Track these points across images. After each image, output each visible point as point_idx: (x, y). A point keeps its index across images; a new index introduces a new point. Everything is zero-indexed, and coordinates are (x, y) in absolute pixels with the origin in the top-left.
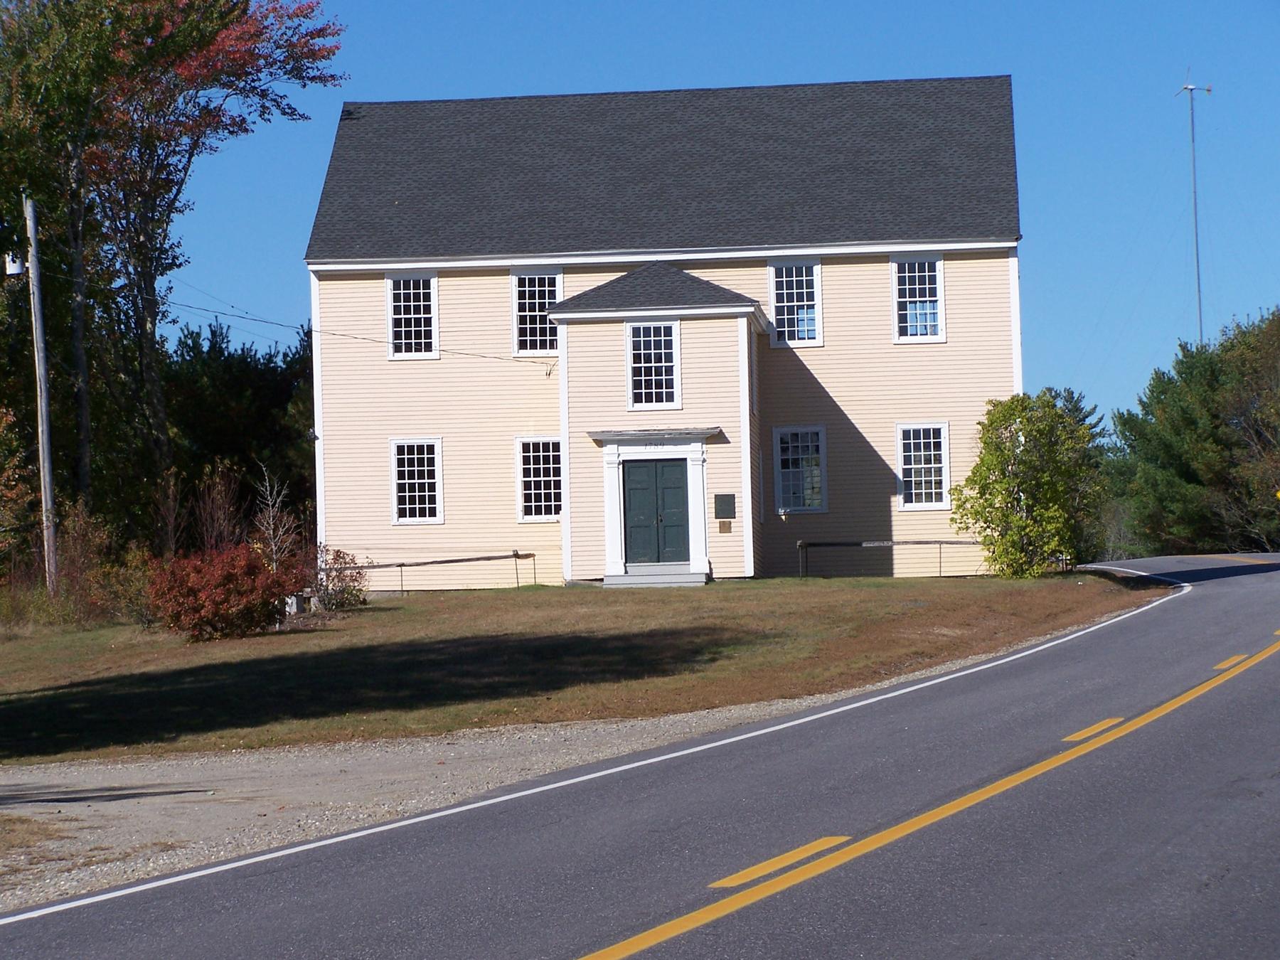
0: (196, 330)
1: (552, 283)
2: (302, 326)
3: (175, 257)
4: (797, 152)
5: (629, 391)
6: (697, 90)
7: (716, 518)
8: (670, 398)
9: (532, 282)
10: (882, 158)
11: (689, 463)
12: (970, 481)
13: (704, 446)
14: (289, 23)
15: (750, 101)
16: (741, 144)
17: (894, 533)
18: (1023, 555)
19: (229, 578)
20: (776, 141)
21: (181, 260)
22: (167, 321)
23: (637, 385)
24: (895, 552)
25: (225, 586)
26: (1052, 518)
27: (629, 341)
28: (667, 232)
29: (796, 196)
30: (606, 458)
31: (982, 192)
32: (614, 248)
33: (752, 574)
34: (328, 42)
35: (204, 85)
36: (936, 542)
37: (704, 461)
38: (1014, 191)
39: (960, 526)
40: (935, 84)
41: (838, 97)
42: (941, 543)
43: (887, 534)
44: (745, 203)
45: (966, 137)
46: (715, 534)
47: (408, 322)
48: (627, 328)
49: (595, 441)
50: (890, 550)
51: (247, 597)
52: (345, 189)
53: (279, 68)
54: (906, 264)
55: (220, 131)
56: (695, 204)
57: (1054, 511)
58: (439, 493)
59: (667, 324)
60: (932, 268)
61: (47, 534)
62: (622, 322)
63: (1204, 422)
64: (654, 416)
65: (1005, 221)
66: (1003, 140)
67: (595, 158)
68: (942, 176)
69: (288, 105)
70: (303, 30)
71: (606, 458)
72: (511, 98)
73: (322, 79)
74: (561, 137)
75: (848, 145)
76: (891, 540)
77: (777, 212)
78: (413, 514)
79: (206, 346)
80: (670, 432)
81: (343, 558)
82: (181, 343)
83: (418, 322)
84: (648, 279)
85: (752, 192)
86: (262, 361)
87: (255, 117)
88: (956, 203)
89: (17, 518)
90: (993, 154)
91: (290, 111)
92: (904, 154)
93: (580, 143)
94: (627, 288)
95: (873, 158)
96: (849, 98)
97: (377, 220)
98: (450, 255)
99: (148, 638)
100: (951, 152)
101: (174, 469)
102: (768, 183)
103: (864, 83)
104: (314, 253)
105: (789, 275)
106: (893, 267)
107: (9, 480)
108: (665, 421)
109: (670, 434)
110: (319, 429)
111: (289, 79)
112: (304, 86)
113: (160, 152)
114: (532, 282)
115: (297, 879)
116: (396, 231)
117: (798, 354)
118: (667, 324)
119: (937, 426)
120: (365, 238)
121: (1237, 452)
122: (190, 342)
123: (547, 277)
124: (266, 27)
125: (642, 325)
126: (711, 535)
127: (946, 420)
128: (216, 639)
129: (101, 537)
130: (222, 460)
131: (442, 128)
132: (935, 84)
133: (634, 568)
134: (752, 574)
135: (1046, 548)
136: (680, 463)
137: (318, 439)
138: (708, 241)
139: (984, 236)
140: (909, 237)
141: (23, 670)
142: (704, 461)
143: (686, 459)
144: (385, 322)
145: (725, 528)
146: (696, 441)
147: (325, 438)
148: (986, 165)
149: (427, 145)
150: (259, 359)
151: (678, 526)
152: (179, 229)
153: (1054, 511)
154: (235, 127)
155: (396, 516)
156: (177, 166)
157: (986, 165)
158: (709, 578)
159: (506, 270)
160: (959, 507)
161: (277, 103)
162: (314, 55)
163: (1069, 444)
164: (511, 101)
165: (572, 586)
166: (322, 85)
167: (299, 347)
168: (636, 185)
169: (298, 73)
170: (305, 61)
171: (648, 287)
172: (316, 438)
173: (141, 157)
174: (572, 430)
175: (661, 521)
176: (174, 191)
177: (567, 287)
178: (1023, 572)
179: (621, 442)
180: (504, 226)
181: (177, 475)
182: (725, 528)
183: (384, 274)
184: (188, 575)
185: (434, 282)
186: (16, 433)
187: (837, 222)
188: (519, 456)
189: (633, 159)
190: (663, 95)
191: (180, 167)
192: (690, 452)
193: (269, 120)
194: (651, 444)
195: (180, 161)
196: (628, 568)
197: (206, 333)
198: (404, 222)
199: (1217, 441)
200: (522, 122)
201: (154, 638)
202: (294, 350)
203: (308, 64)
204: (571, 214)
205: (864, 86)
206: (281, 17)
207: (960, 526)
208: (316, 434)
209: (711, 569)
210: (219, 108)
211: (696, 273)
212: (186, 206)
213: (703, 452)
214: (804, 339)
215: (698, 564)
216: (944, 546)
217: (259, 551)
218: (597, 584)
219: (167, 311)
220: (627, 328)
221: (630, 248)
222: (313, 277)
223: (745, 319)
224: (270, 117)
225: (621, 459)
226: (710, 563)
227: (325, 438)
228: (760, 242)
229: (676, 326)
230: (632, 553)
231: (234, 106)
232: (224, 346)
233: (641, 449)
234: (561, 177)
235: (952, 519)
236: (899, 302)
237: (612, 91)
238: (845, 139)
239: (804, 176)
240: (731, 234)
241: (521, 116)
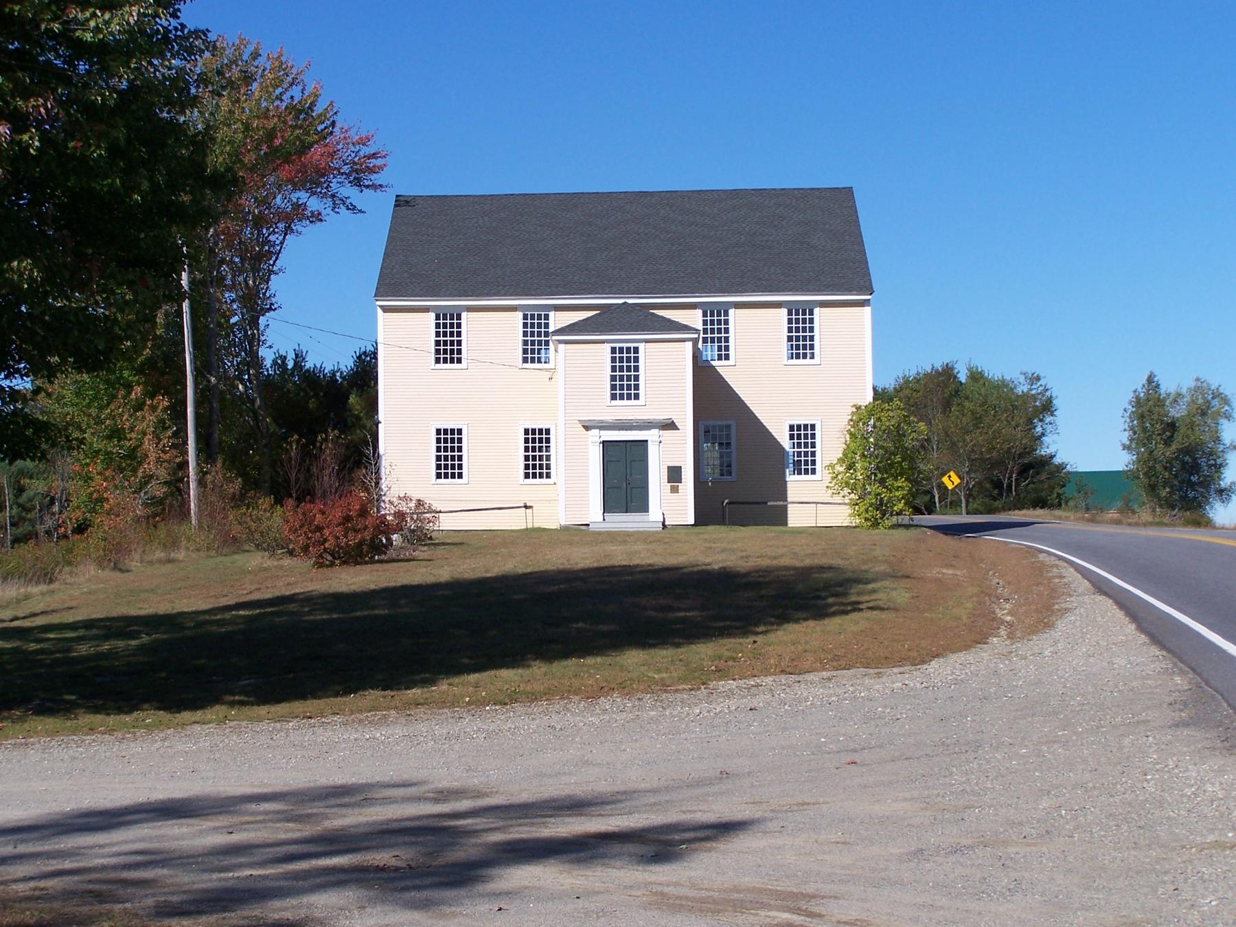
0: (284, 354)
1: (547, 317)
5: (608, 392)
9: (533, 317)
10: (771, 238)
12: (841, 461)
14: (353, 149)
19: (348, 519)
20: (697, 226)
21: (276, 306)
23: (613, 387)
24: (789, 509)
25: (344, 525)
26: (900, 487)
27: (609, 356)
30: (591, 439)
32: (582, 294)
33: (693, 523)
34: (379, 162)
36: (813, 503)
37: (660, 442)
42: (818, 503)
43: (785, 499)
47: (445, 343)
48: (608, 347)
49: (583, 426)
50: (786, 507)
54: (792, 309)
55: (304, 221)
57: (901, 482)
59: (636, 345)
61: (192, 485)
62: (604, 343)
64: (625, 410)
66: (853, 228)
70: (362, 154)
71: (591, 439)
76: (786, 501)
79: (290, 365)
81: (423, 505)
82: (275, 362)
83: (452, 343)
87: (329, 210)
88: (826, 269)
89: (169, 474)
90: (847, 238)
93: (561, 225)
101: (296, 437)
104: (380, 292)
107: (164, 446)
112: (361, 191)
113: (265, 231)
114: (533, 317)
118: (636, 345)
122: (279, 362)
124: (338, 150)
125: (618, 345)
127: (820, 418)
130: (333, 431)
132: (801, 191)
133: (609, 516)
135: (895, 508)
136: (642, 443)
139: (849, 291)
141: (185, 588)
142: (660, 442)
143: (647, 441)
145: (675, 490)
152: (277, 285)
160: (833, 478)
162: (372, 170)
165: (565, 529)
166: (373, 191)
169: (358, 183)
172: (379, 422)
174: (567, 418)
176: (274, 258)
177: (558, 320)
180: (512, 278)
182: (675, 490)
184: (315, 516)
185: (464, 315)
186: (168, 415)
189: (599, 236)
191: (278, 242)
192: (651, 435)
194: (623, 429)
201: (281, 562)
204: (558, 271)
205: (753, 192)
206: (348, 144)
208: (380, 419)
209: (664, 519)
215: (655, 514)
216: (818, 505)
220: (608, 347)
222: (380, 311)
225: (602, 439)
228: (692, 291)
229: (641, 346)
230: (608, 507)
231: (314, 204)
233: (617, 432)
235: (827, 487)
236: (611, 376)
238: (744, 225)
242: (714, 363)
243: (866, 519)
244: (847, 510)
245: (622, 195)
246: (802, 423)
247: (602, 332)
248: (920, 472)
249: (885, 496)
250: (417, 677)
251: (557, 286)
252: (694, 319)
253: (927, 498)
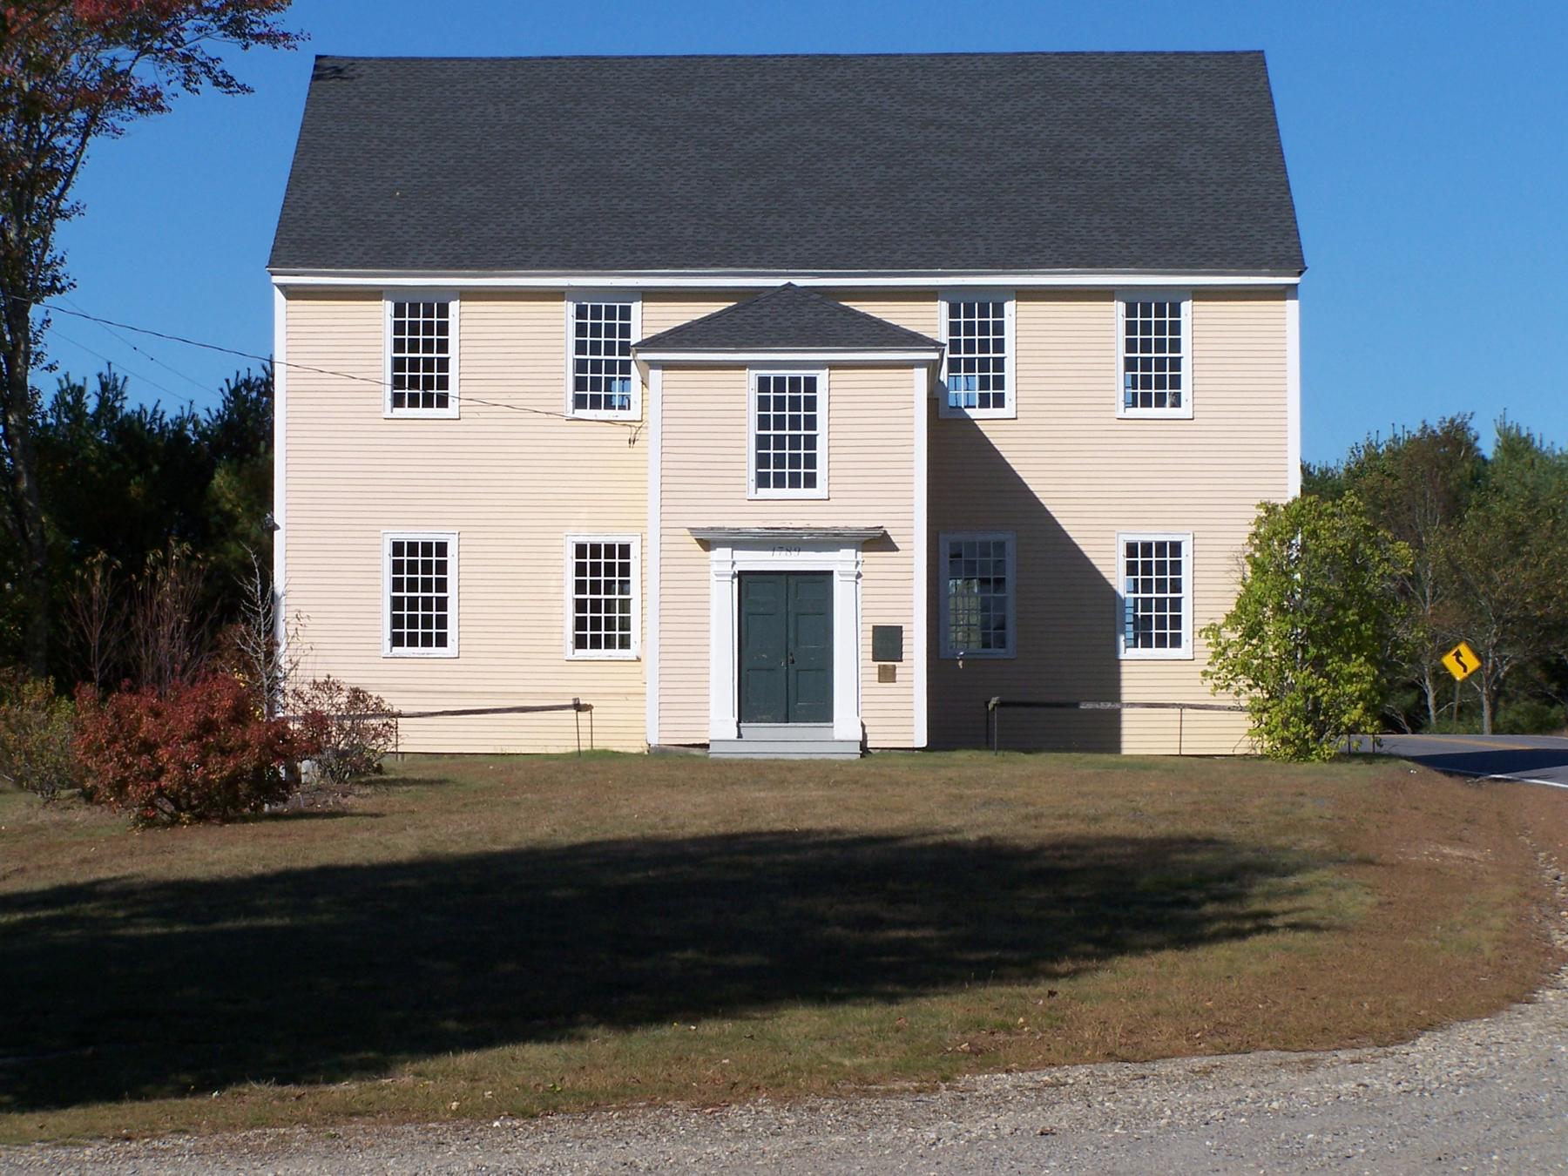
0: (80, 383)
1: (626, 313)
2: (227, 381)
3: (55, 278)
4: (971, 144)
6: (820, 55)
7: (874, 660)
8: (811, 481)
9: (596, 313)
10: (1093, 155)
11: (836, 578)
12: (1233, 619)
13: (859, 553)
15: (896, 73)
16: (888, 129)
17: (1124, 690)
18: (1309, 727)
19: (208, 727)
20: (939, 128)
21: (64, 281)
22: (41, 366)
23: (762, 461)
24: (1124, 718)
25: (200, 738)
26: (1355, 675)
28: (793, 247)
29: (975, 203)
30: (715, 568)
31: (1243, 207)
35: (109, 39)
36: (1174, 706)
37: (859, 576)
38: (1286, 206)
39: (1216, 682)
40: (1159, 59)
41: (1020, 72)
42: (1182, 706)
44: (902, 210)
45: (1211, 132)
46: (872, 684)
48: (751, 377)
50: (1117, 715)
51: (235, 758)
52: (323, 172)
53: (212, 20)
54: (1136, 302)
55: (125, 108)
56: (829, 209)
57: (1357, 665)
58: (451, 613)
60: (1176, 311)
65: (1281, 248)
67: (680, 142)
68: (1182, 183)
69: (222, 72)
71: (715, 568)
72: (555, 58)
73: (272, 38)
74: (631, 112)
75: (1043, 136)
77: (950, 224)
78: (413, 641)
79: (91, 405)
80: (811, 531)
82: (59, 400)
84: (780, 309)
85: (911, 196)
86: (170, 426)
87: (177, 86)
91: (225, 81)
92: (1124, 151)
94: (750, 320)
95: (1082, 155)
96: (1038, 74)
97: (371, 217)
98: (479, 268)
99: (56, 817)
100: (1191, 151)
101: (102, 555)
102: (934, 184)
103: (1057, 54)
106: (1120, 307)
108: (802, 516)
109: (811, 535)
110: (279, 515)
111: (225, 36)
112: (246, 47)
113: (43, 126)
114: (596, 313)
116: (399, 233)
117: (982, 428)
119: (1176, 539)
120: (354, 241)
122: (69, 398)
123: (618, 305)
125: (772, 373)
126: (866, 684)
127: (1189, 530)
128: (184, 823)
129: (1500, 444)
130: (178, 543)
131: (459, 94)
132: (1159, 59)
133: (753, 730)
134: (925, 745)
137: (278, 528)
138: (855, 261)
140: (1146, 265)
142: (859, 576)
144: (382, 362)
145: (887, 676)
146: (847, 545)
147: (289, 527)
148: (1244, 170)
149: (437, 116)
150: (167, 424)
151: (818, 670)
154: (146, 103)
155: (388, 643)
156: (64, 149)
157: (1244, 170)
158: (864, 749)
159: (558, 293)
160: (1216, 655)
161: (209, 68)
164: (555, 61)
165: (659, 754)
167: (222, 409)
168: (743, 180)
169: (237, 29)
170: (249, 12)
171: (780, 320)
173: (16, 132)
175: (793, 662)
176: (60, 184)
178: (1310, 751)
180: (556, 230)
181: (106, 565)
182: (887, 676)
183: (381, 292)
184: (139, 720)
185: (454, 306)
187: (1038, 240)
188: (570, 562)
189: (736, 145)
190: (771, 61)
192: (839, 562)
193: (197, 91)
194: (781, 549)
195: (69, 143)
196: (742, 731)
197: (93, 387)
198: (412, 221)
200: (574, 90)
202: (214, 414)
203: (251, 17)
204: (652, 217)
207: (1216, 682)
209: (864, 735)
210: (126, 72)
212: (75, 209)
213: (858, 563)
214: (974, 407)
215: (845, 725)
217: (242, 685)
218: (696, 751)
219: (42, 352)
220: (751, 377)
221: (742, 266)
222: (279, 296)
223: (925, 370)
224: (198, 86)
225: (737, 569)
226: (863, 726)
227: (289, 527)
229: (822, 377)
231: (146, 72)
232: (118, 404)
234: (634, 166)
235: (1205, 673)
237: (698, 53)
239: (984, 176)
240: (886, 253)
241: (570, 82)
243: (1284, 741)
244: (1245, 722)
248: (1397, 646)
249: (1324, 693)
252: (933, 320)
253: (1410, 698)
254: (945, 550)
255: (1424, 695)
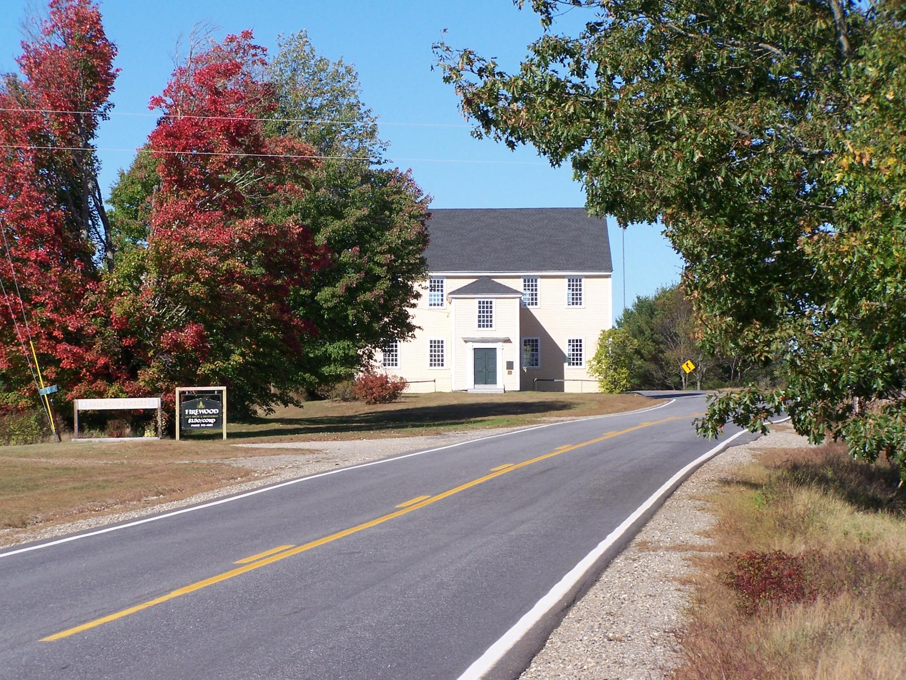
27: (478, 305)
50: (563, 382)
54: (571, 279)
57: (624, 370)
63: (648, 333)
64: (486, 333)
105: (529, 282)
115: (895, 330)
121: (662, 346)
125: (482, 300)
133: (477, 386)
139: (600, 270)
145: (510, 373)
153: (624, 370)
158: (505, 392)
163: (631, 346)
179: (473, 342)
182: (510, 373)
199: (654, 341)
211: (495, 280)
220: (477, 301)
229: (494, 301)
242: (529, 307)
243: (607, 389)
244: (597, 384)
245: (479, 211)
246: (575, 338)
247: (474, 293)
248: (634, 365)
249: (617, 377)
250: (472, 419)
251: (448, 266)
252: (517, 284)
253: (677, 379)
254: (523, 341)
255: (681, 379)
